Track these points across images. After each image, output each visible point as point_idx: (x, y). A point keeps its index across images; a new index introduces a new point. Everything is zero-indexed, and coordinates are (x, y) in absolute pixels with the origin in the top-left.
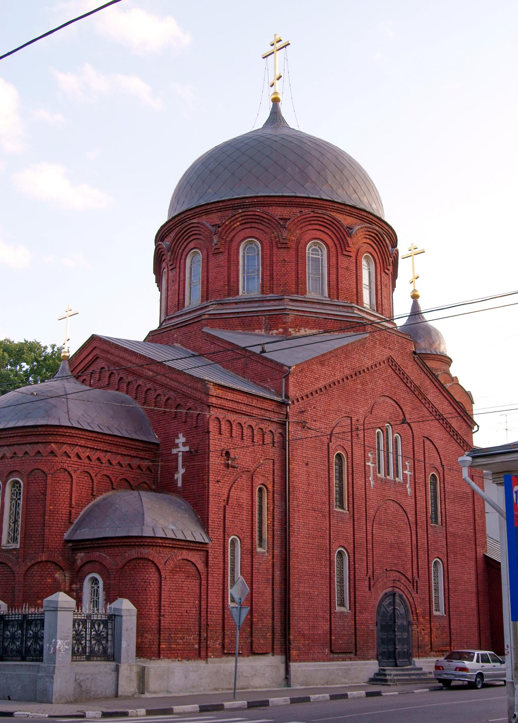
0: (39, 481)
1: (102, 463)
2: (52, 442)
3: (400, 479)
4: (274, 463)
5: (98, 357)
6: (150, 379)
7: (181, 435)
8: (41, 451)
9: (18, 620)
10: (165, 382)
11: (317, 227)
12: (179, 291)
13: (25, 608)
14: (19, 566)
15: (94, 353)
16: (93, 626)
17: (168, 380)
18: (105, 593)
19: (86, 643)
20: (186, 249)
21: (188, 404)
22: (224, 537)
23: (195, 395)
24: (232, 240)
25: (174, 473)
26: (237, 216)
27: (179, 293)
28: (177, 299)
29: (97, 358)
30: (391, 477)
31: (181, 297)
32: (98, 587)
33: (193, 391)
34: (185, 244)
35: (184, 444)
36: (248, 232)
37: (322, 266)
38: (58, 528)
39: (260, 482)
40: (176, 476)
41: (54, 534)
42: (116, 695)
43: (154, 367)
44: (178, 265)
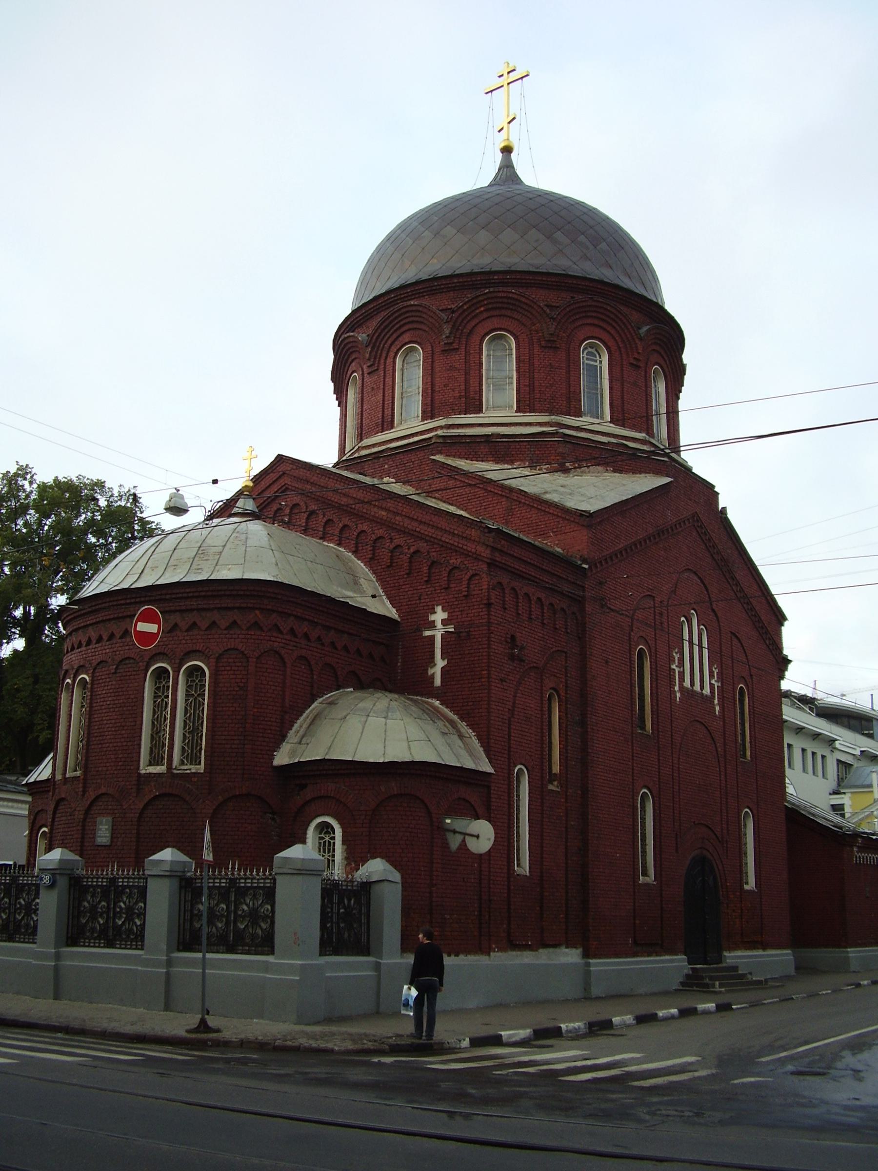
0: (236, 668)
1: (323, 644)
2: (257, 609)
3: (707, 691)
4: (566, 657)
5: (287, 489)
6: (381, 523)
7: (439, 609)
8: (238, 621)
9: (220, 887)
10: (410, 527)
11: (596, 322)
12: (383, 403)
13: (233, 868)
14: (204, 802)
15: (282, 482)
16: (341, 902)
17: (415, 524)
18: (345, 847)
19: (332, 926)
20: (396, 343)
21: (451, 562)
22: (509, 766)
23: (465, 547)
24: (471, 331)
25: (428, 666)
26: (480, 298)
27: (383, 406)
28: (380, 415)
29: (285, 489)
30: (697, 687)
31: (388, 412)
32: (334, 838)
33: (461, 541)
34: (395, 336)
35: (444, 622)
36: (496, 322)
37: (601, 378)
38: (265, 744)
39: (552, 685)
40: (430, 672)
41: (259, 752)
42: (378, 1013)
43: (390, 504)
44: (382, 367)
